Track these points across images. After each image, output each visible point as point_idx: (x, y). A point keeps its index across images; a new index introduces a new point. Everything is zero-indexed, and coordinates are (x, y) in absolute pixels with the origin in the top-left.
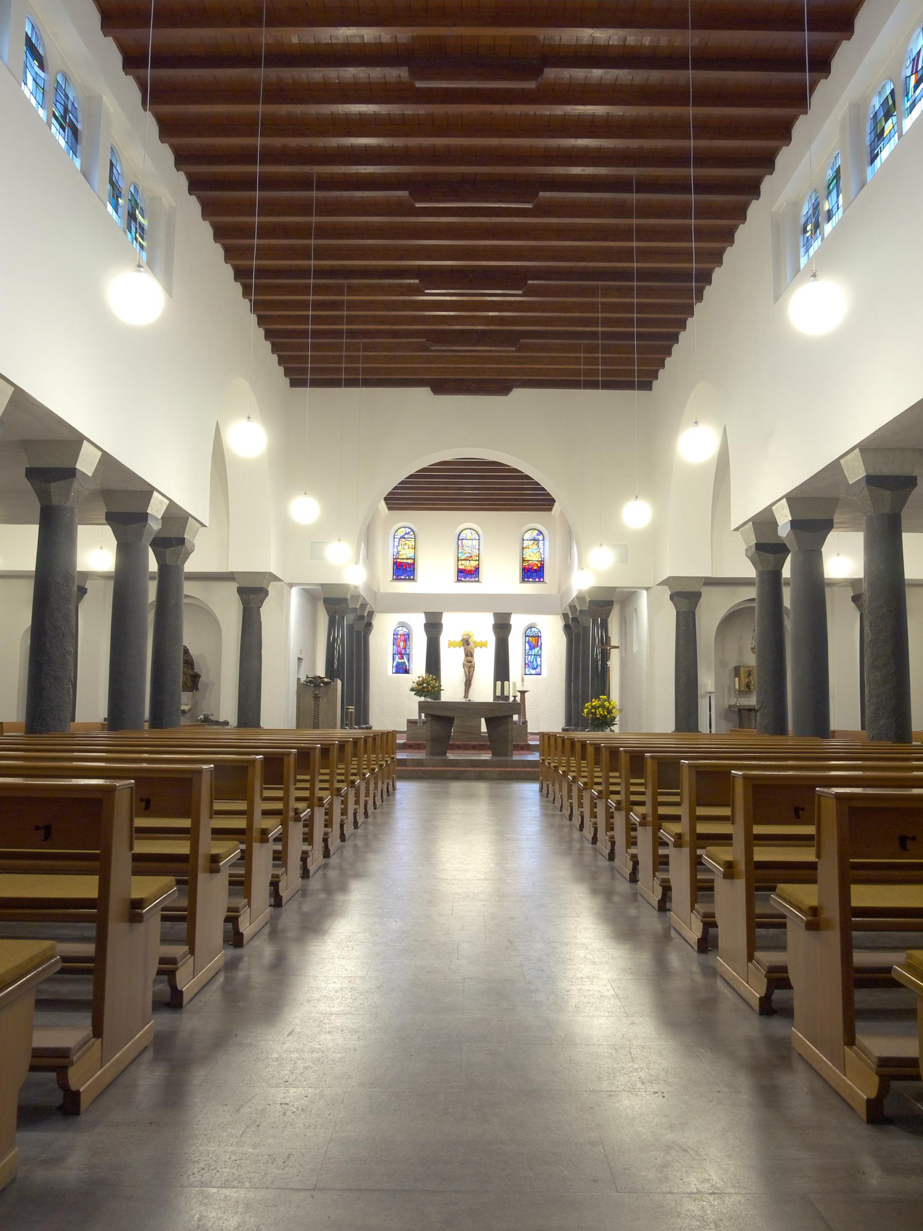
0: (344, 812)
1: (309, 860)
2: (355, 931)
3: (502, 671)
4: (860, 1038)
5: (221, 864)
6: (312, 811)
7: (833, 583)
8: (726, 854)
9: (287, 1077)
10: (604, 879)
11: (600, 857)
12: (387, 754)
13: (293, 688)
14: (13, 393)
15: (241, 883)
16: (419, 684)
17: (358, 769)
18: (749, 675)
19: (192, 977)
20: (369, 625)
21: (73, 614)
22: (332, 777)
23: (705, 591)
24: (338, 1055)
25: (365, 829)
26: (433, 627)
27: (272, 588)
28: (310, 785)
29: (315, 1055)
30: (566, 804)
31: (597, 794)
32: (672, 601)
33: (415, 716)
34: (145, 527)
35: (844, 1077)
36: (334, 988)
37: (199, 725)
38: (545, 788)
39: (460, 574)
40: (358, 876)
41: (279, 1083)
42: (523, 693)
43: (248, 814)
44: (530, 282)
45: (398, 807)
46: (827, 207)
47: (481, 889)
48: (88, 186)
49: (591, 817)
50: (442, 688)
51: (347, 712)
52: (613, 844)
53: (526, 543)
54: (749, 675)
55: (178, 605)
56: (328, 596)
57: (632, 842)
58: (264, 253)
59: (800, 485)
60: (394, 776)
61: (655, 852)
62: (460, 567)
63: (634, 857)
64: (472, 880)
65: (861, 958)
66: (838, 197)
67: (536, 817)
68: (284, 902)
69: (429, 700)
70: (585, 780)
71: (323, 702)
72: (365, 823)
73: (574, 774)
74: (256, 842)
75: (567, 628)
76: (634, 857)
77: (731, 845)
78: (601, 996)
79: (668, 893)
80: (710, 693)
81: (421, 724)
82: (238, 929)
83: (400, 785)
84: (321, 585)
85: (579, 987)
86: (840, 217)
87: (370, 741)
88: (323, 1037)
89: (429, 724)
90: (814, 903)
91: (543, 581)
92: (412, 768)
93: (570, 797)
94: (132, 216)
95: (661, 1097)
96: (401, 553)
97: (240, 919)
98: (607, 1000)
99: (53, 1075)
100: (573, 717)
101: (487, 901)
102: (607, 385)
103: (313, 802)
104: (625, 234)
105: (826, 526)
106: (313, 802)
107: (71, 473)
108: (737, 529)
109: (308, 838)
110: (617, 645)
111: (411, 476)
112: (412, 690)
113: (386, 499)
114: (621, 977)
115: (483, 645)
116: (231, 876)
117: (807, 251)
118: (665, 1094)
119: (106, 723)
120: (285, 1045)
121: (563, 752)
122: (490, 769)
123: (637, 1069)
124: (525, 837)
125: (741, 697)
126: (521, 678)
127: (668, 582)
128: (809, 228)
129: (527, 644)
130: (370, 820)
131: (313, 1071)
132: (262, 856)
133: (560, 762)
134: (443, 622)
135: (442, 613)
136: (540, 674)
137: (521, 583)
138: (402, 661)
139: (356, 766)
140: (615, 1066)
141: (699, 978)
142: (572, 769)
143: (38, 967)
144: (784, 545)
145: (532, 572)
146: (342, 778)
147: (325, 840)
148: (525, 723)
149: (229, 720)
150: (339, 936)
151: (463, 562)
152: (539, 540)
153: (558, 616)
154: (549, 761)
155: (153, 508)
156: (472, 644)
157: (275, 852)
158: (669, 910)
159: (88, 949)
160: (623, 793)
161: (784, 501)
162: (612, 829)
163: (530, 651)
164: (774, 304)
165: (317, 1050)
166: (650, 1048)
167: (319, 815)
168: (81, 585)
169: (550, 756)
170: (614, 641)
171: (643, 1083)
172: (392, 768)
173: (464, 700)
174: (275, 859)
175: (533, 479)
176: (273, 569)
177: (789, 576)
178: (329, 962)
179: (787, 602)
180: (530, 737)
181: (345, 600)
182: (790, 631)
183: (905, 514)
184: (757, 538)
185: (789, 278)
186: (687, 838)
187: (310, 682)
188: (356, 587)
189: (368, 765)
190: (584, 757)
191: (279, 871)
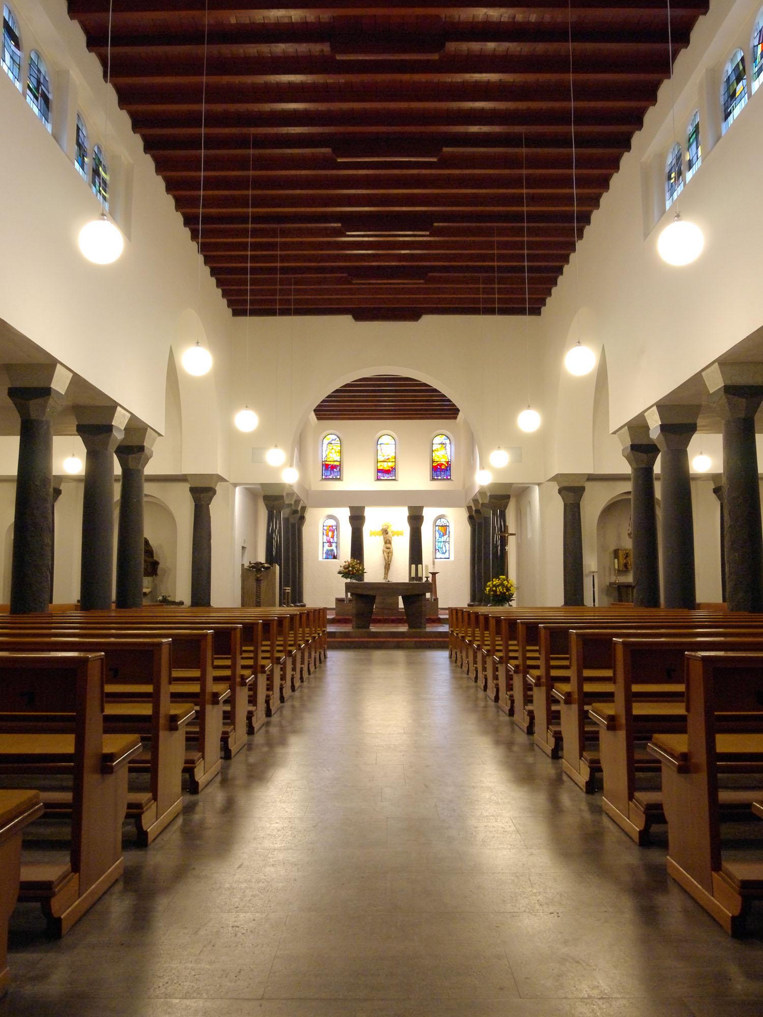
0: (283, 678)
1: (254, 719)
2: (294, 778)
6: (256, 678)
7: (698, 478)
8: (609, 709)
9: (237, 904)
10: (505, 731)
11: (501, 713)
18: (627, 557)
20: (302, 518)
21: (50, 511)
23: (588, 486)
25: (301, 692)
26: (357, 520)
27: (219, 488)
29: (261, 885)
30: (472, 668)
34: (110, 436)
35: (712, 898)
36: (276, 828)
39: (379, 474)
40: (294, 732)
41: (231, 909)
42: (434, 574)
43: (201, 680)
44: (436, 224)
45: (329, 673)
46: (688, 158)
51: (284, 593)
52: (513, 702)
53: (435, 447)
54: (627, 557)
55: (139, 502)
57: (528, 700)
58: (209, 202)
60: (325, 646)
63: (531, 714)
64: (393, 734)
65: (725, 796)
66: (697, 148)
68: (233, 754)
69: (354, 581)
70: (488, 648)
71: (264, 584)
72: (301, 687)
75: (471, 518)
76: (531, 714)
77: (613, 701)
80: (593, 572)
87: (304, 617)
88: (268, 869)
89: (354, 602)
93: (475, 662)
94: (96, 173)
95: (556, 917)
96: (328, 457)
97: (196, 770)
99: (38, 905)
100: (478, 594)
103: (257, 669)
104: (517, 182)
105: (689, 429)
106: (257, 669)
107: (47, 391)
108: (614, 433)
109: (253, 700)
110: (514, 533)
111: (337, 391)
112: (340, 573)
113: (315, 411)
115: (399, 534)
116: (187, 733)
117: (672, 195)
118: (560, 915)
122: (407, 639)
123: (536, 893)
124: (437, 697)
127: (556, 478)
128: (673, 175)
129: (437, 532)
130: (305, 684)
132: (214, 717)
133: (466, 632)
135: (364, 507)
137: (431, 480)
138: (331, 548)
140: (517, 890)
141: (587, 816)
142: (477, 638)
144: (656, 445)
145: (439, 470)
148: (436, 600)
151: (382, 463)
153: (464, 509)
156: (390, 533)
157: (225, 712)
160: (520, 658)
161: (655, 408)
172: (323, 639)
173: (384, 581)
176: (220, 472)
179: (658, 494)
180: (440, 612)
181: (281, 497)
186: (576, 696)
187: (253, 567)
188: (291, 486)
189: (303, 637)
190: (487, 628)
191: (229, 729)
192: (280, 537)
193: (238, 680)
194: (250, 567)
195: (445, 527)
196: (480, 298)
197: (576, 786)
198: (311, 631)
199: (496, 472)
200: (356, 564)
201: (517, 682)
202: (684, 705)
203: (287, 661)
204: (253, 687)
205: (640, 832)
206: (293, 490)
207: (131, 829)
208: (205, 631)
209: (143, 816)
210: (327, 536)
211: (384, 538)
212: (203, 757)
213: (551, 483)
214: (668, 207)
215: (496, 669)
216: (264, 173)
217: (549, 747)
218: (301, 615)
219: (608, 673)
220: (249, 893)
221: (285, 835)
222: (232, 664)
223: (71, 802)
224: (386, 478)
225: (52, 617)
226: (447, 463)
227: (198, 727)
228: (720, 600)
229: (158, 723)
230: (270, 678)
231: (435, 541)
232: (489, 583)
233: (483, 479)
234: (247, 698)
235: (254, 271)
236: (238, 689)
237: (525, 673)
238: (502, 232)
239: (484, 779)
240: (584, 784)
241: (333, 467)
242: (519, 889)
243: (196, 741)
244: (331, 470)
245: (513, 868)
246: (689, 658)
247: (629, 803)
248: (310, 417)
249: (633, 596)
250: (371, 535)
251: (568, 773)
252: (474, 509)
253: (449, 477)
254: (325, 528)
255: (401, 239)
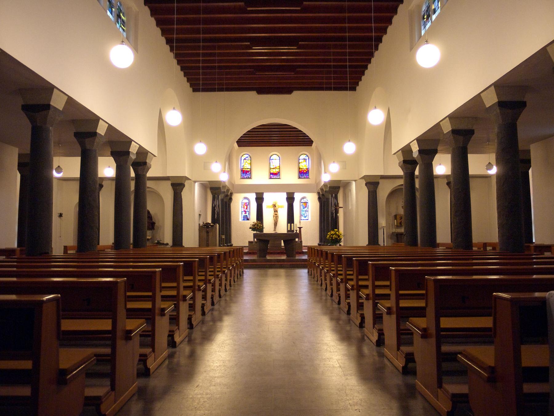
0: (220, 285)
1: (205, 307)
2: (226, 339)
3: (290, 219)
4: (444, 385)
5: (166, 312)
6: (206, 286)
7: (439, 177)
8: (388, 304)
9: (196, 406)
10: (336, 313)
11: (334, 303)
12: (239, 257)
13: (197, 228)
14: (67, 99)
15: (175, 319)
16: (253, 225)
17: (227, 265)
18: (401, 219)
19: (154, 361)
20: (231, 199)
21: (97, 197)
22: (215, 270)
23: (381, 181)
24: (218, 396)
25: (230, 292)
26: (260, 200)
27: (187, 183)
28: (205, 273)
29: (208, 396)
30: (319, 279)
31: (332, 275)
32: (366, 186)
33: (252, 240)
34: (128, 157)
35: (438, 402)
36: (216, 366)
37: (155, 246)
38: (310, 271)
39: (271, 175)
40: (227, 314)
41: (193, 409)
42: (300, 228)
43: (177, 288)
44: (300, 43)
45: (245, 281)
46: (433, 7)
47: (281, 319)
48: (99, 4)
49: (330, 285)
50: (264, 227)
51: (221, 238)
52: (340, 297)
53: (300, 161)
54: (401, 219)
55: (144, 190)
56: (212, 186)
57: (347, 296)
58: (179, 31)
59: (423, 134)
60: (243, 267)
61: (358, 301)
62: (271, 172)
63: (349, 304)
64: (277, 315)
65: (445, 348)
66: (438, 3)
67: (306, 285)
68: (194, 326)
69: (258, 232)
70: (327, 269)
71: (210, 234)
72: (230, 289)
73: (322, 266)
74: (181, 301)
75: (319, 199)
76: (349, 304)
77: (390, 299)
78: (333, 367)
79: (364, 320)
80: (384, 227)
81: (255, 243)
82: (174, 340)
83: (245, 271)
84: (209, 181)
85: (324, 363)
86: (439, 12)
87: (231, 253)
88: (211, 388)
89: (258, 244)
90: (425, 326)
91: (308, 178)
92: (251, 263)
93: (321, 276)
94: (119, 16)
95: (358, 412)
96: (244, 166)
97: (175, 335)
98: (336, 369)
99: (94, 407)
100: (323, 239)
101: (284, 324)
102: (336, 89)
103: (206, 282)
104: (343, 20)
105: (434, 152)
106: (206, 282)
107: (95, 134)
108: (394, 154)
109: (204, 298)
110: (342, 206)
111: (249, 131)
112: (250, 228)
113: (237, 142)
114: (342, 358)
115: (282, 207)
116: (170, 315)
117: (425, 27)
118: (360, 411)
119: (113, 245)
120: (195, 392)
121: (318, 256)
122: (286, 263)
123: (348, 399)
124: (301, 294)
125: (397, 228)
126: (299, 222)
127: (364, 177)
128: (425, 17)
129: (302, 206)
130: (232, 288)
131: (208, 403)
132: (184, 307)
133: (316, 260)
134: (264, 197)
135: (263, 193)
136: (308, 220)
137: (298, 179)
138: (246, 215)
139: (225, 264)
140: (339, 398)
141: (377, 358)
142: (322, 263)
143: (87, 361)
144: (415, 160)
145: (303, 174)
146: (219, 270)
147: (212, 298)
148: (301, 242)
149: (169, 243)
150: (218, 342)
152: (306, 159)
153: (316, 193)
154: (312, 260)
155: (132, 149)
156: (277, 207)
157: (190, 304)
158: (364, 327)
159: (108, 351)
160: (344, 275)
161: (415, 141)
162: (339, 291)
163: (303, 209)
164: (410, 52)
165: (209, 394)
166: (354, 390)
167: (209, 287)
168: (101, 183)
169: (312, 257)
170: (341, 204)
171: (351, 406)
172: (242, 264)
173: (273, 232)
174: (189, 307)
175: (303, 132)
176: (187, 175)
177: (418, 174)
178: (214, 353)
179: (417, 186)
180: (304, 248)
181: (219, 188)
182: (418, 197)
183: (469, 146)
184: (404, 158)
185: (417, 39)
186: (371, 296)
187: (205, 225)
188: (224, 182)
189: (231, 263)
190: (327, 259)
191: (192, 313)
192: (219, 209)
193: (197, 287)
194: (204, 225)
195: (306, 203)
196: (324, 82)
197: (371, 342)
198: (235, 259)
199: (332, 174)
200: (259, 224)
201: (342, 286)
202: (425, 301)
203: (222, 276)
204: (205, 291)
205: (403, 367)
206: (225, 184)
207: (141, 366)
208: (179, 263)
209: (148, 361)
210: (244, 208)
211: (274, 209)
212: (179, 328)
213: (361, 180)
214: (423, 34)
215: (331, 280)
216: (208, 16)
217: (358, 322)
218: (229, 252)
219: (388, 283)
220: (202, 400)
221: (220, 369)
222: (193, 279)
223: (110, 354)
224: (275, 177)
225: (99, 254)
226: (307, 169)
227: (176, 312)
228: (450, 242)
229: (155, 312)
230: (213, 285)
231: (301, 211)
232: (329, 233)
233: (326, 178)
234: (201, 296)
235: (203, 68)
236: (197, 292)
237: (346, 283)
238: (335, 47)
239: (324, 339)
240: (375, 341)
241: (247, 172)
242: (340, 397)
243: (174, 320)
244: (246, 173)
245: (337, 386)
246: (427, 279)
247: (397, 353)
248: (234, 145)
249: (404, 239)
250: (267, 208)
251: (368, 335)
252: (321, 193)
253: (308, 177)
254: (243, 204)
255: (282, 51)
